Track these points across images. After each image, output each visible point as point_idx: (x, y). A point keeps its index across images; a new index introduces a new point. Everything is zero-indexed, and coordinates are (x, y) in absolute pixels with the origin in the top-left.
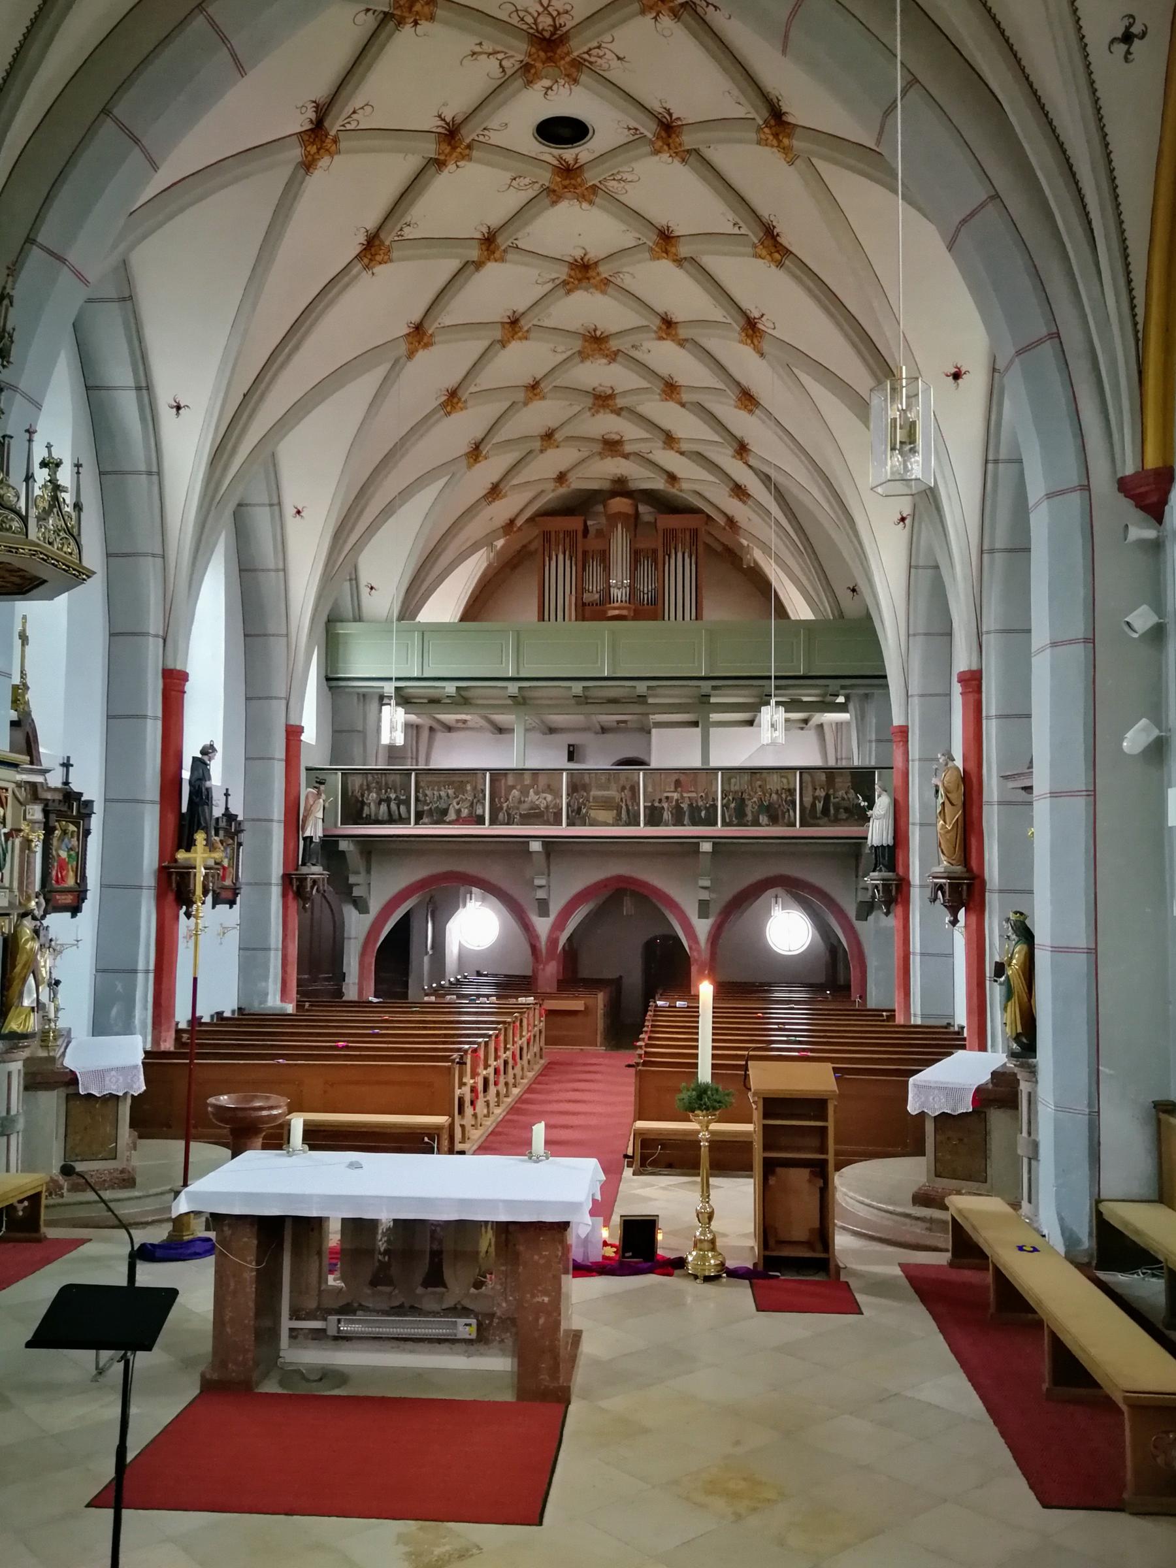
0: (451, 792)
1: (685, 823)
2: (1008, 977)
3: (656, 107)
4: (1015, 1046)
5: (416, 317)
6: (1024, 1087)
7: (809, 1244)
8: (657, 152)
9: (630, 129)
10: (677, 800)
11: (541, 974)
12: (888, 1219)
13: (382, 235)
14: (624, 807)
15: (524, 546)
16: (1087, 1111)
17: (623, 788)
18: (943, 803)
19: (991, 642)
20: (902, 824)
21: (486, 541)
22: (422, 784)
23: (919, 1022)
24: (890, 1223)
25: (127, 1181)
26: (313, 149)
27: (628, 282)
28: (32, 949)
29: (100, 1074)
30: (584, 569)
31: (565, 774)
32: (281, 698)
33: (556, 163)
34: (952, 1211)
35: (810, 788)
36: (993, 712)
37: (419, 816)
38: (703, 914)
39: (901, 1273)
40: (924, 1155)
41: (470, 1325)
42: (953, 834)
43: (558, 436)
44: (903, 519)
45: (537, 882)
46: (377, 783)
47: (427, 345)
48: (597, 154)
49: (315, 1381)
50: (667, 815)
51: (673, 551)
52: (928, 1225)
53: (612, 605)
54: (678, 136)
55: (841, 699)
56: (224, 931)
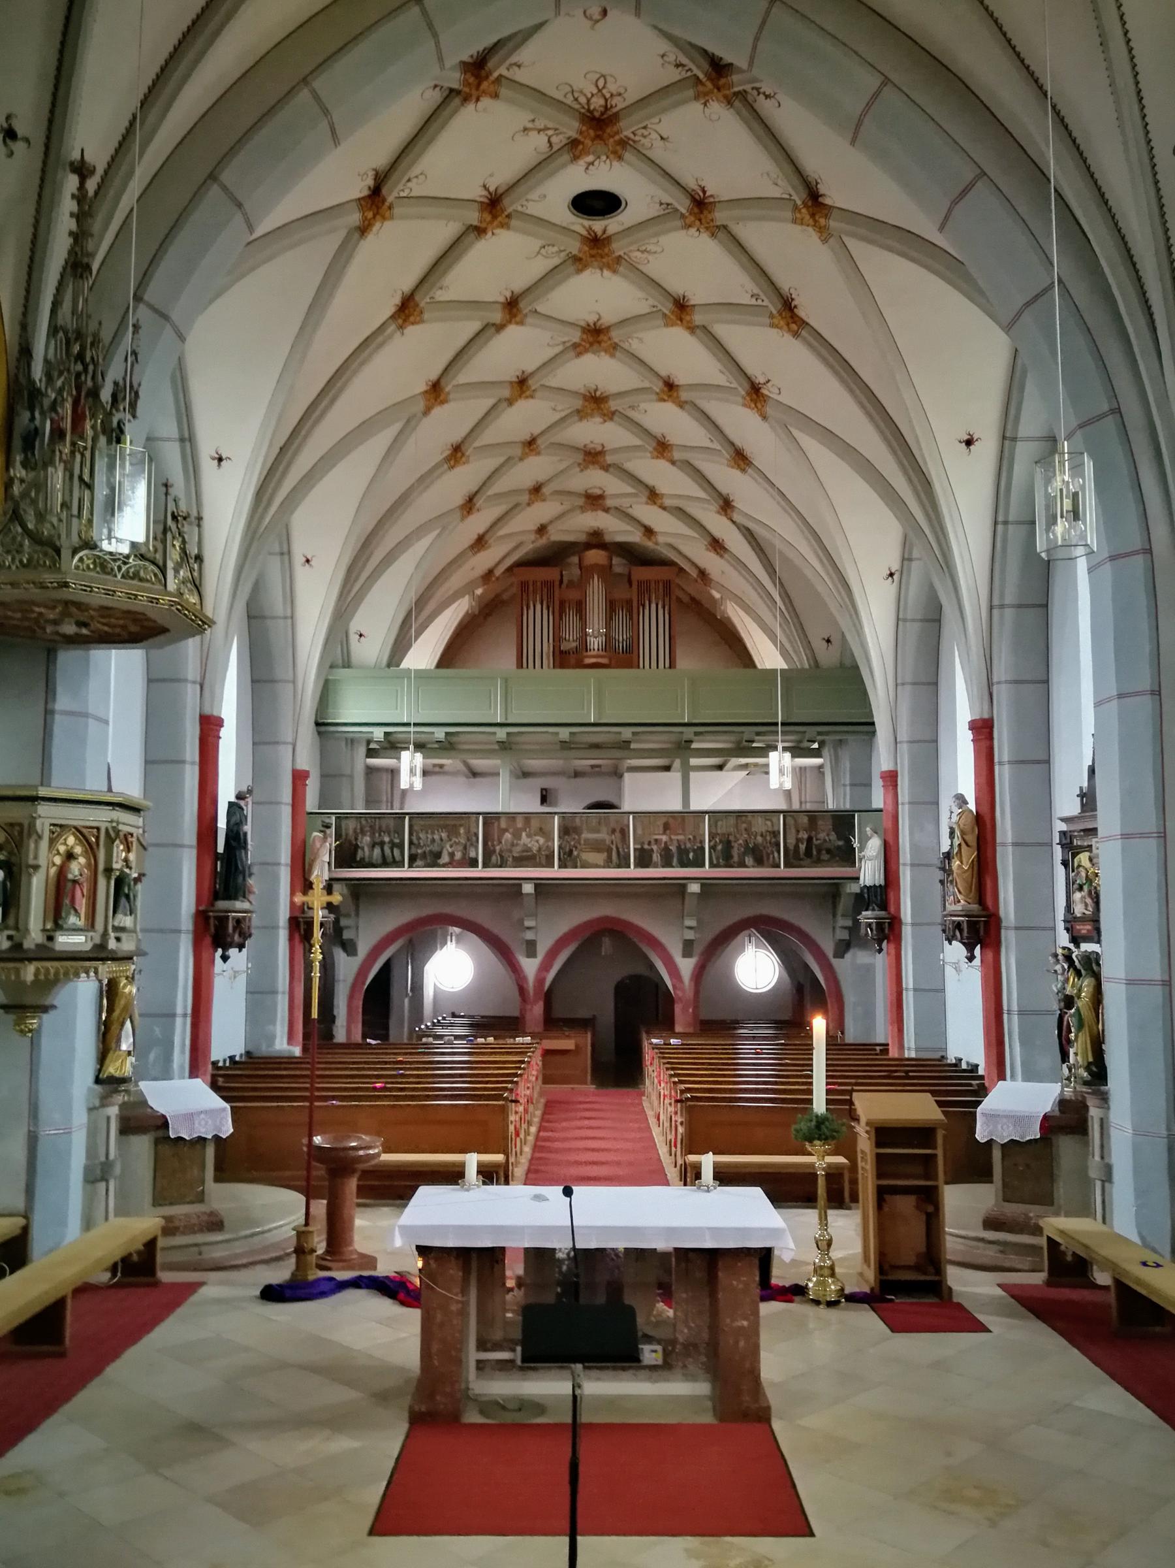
0: (444, 835)
1: (674, 864)
2: (1078, 1010)
3: (692, 184)
4: (1085, 1074)
5: (434, 376)
6: (1094, 1112)
7: (917, 1268)
8: (688, 226)
9: (661, 204)
10: (666, 843)
11: (528, 1017)
12: (962, 1244)
13: (417, 298)
14: (614, 849)
15: (497, 596)
16: (1164, 1133)
17: (614, 831)
18: (960, 845)
19: (1003, 693)
20: (893, 866)
21: (468, 589)
22: (416, 828)
23: (913, 1055)
24: (962, 1247)
25: (215, 1224)
26: (370, 215)
27: (635, 346)
28: (130, 993)
29: (190, 1117)
30: (561, 619)
31: (556, 817)
32: (287, 743)
33: (584, 233)
34: (1047, 1231)
35: (793, 831)
36: (1006, 758)
37: (413, 859)
38: (687, 954)
39: (1004, 1293)
40: (991, 1182)
41: (655, 1351)
42: (970, 873)
43: (546, 490)
44: (891, 575)
45: (527, 923)
46: (371, 827)
47: (443, 402)
48: (626, 226)
49: (514, 1410)
50: (656, 857)
51: (647, 602)
52: (1002, 1248)
53: (589, 653)
54: (710, 212)
55: (816, 746)
56: (236, 974)
